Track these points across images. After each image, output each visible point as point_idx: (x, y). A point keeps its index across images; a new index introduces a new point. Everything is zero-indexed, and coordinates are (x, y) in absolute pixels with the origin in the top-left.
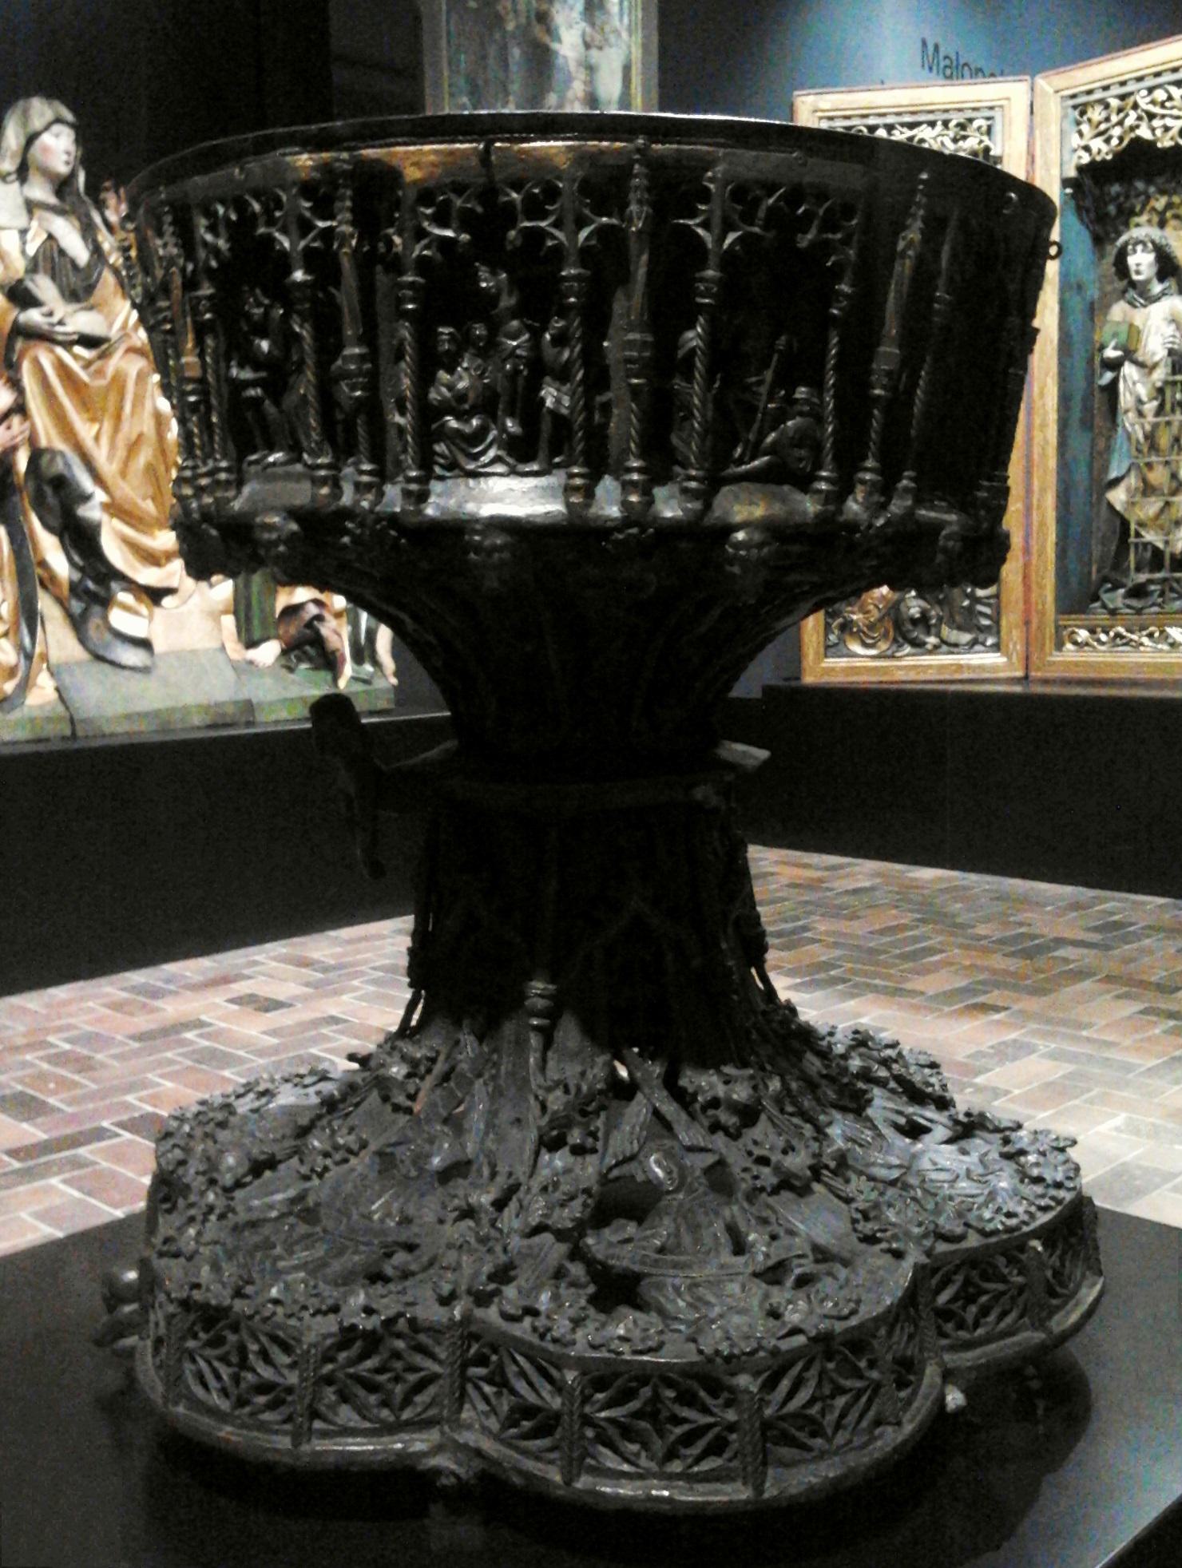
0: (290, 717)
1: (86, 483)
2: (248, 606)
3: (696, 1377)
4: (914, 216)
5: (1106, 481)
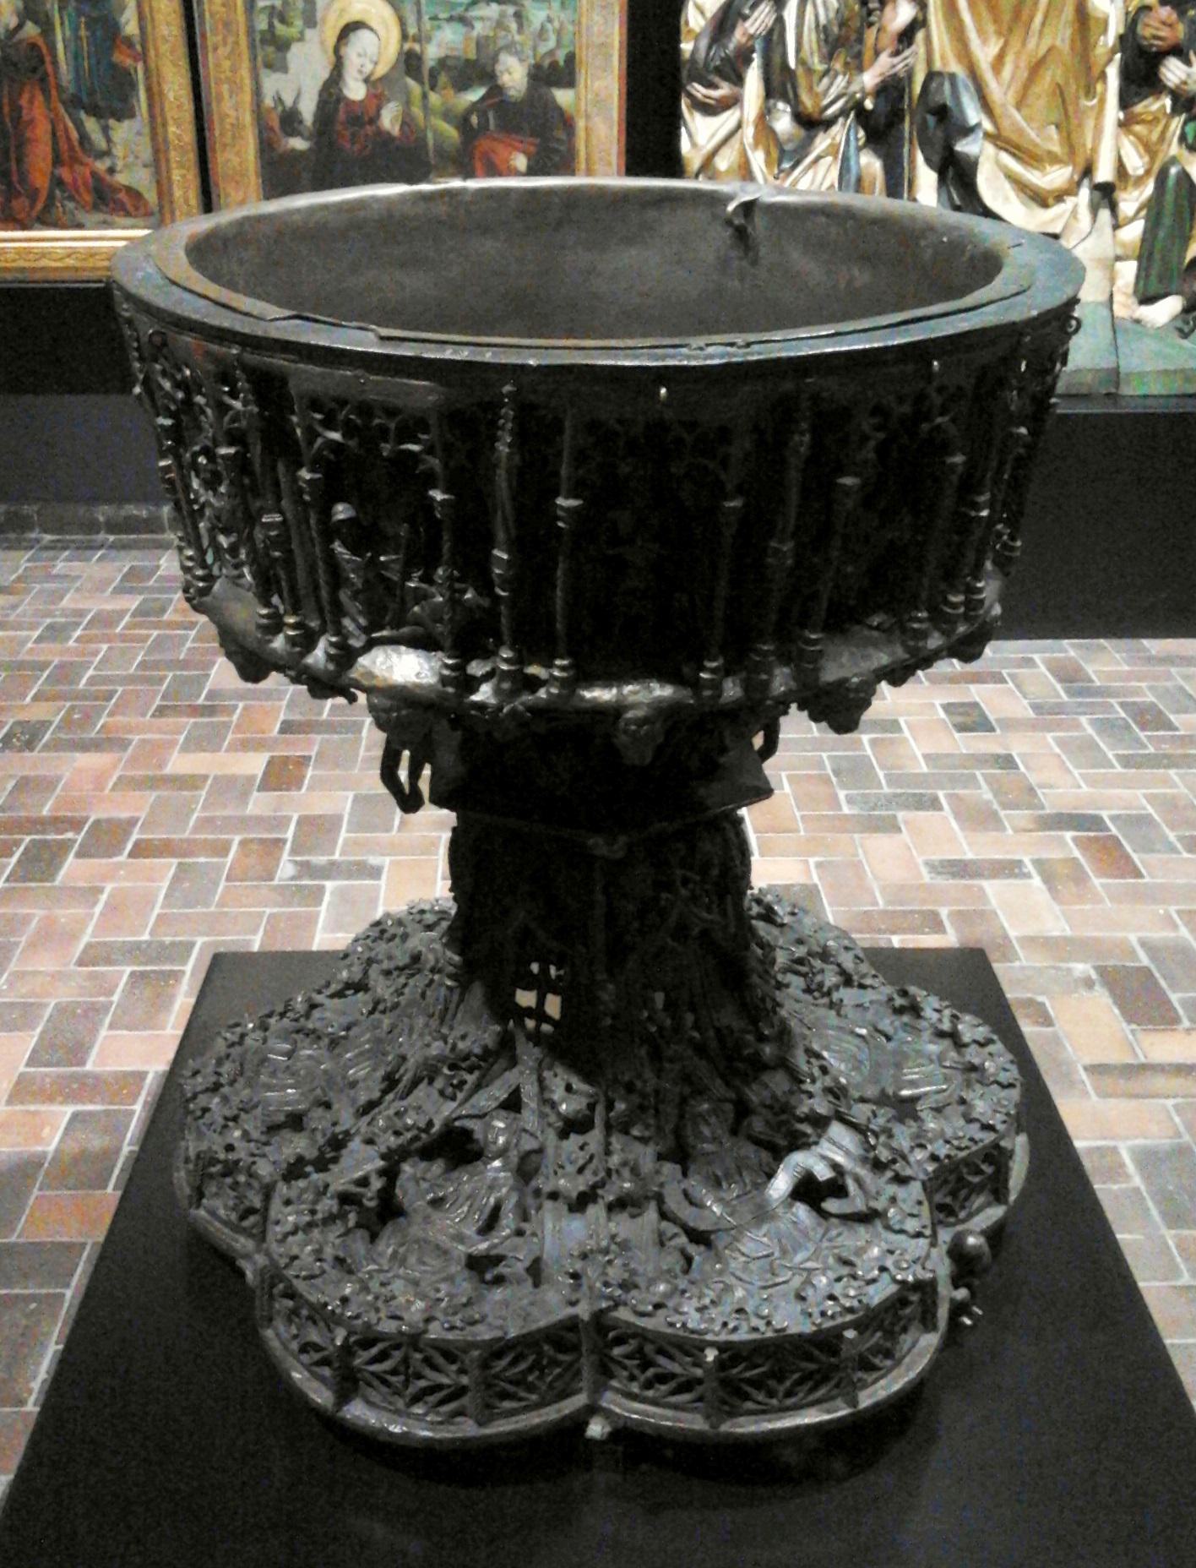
0: (1164, 392)
1: (973, 114)
2: (1151, 254)
3: (436, 1348)
4: (502, 428)
5: (495, 680)
